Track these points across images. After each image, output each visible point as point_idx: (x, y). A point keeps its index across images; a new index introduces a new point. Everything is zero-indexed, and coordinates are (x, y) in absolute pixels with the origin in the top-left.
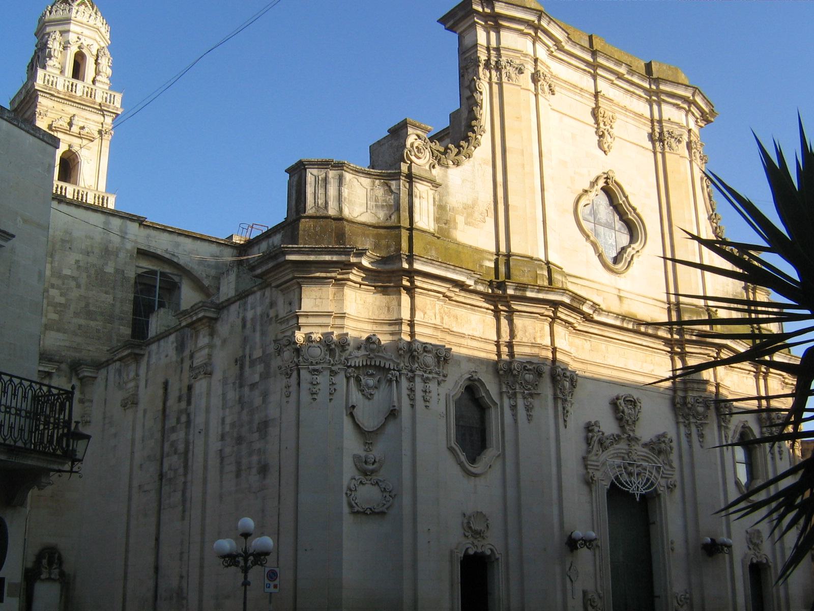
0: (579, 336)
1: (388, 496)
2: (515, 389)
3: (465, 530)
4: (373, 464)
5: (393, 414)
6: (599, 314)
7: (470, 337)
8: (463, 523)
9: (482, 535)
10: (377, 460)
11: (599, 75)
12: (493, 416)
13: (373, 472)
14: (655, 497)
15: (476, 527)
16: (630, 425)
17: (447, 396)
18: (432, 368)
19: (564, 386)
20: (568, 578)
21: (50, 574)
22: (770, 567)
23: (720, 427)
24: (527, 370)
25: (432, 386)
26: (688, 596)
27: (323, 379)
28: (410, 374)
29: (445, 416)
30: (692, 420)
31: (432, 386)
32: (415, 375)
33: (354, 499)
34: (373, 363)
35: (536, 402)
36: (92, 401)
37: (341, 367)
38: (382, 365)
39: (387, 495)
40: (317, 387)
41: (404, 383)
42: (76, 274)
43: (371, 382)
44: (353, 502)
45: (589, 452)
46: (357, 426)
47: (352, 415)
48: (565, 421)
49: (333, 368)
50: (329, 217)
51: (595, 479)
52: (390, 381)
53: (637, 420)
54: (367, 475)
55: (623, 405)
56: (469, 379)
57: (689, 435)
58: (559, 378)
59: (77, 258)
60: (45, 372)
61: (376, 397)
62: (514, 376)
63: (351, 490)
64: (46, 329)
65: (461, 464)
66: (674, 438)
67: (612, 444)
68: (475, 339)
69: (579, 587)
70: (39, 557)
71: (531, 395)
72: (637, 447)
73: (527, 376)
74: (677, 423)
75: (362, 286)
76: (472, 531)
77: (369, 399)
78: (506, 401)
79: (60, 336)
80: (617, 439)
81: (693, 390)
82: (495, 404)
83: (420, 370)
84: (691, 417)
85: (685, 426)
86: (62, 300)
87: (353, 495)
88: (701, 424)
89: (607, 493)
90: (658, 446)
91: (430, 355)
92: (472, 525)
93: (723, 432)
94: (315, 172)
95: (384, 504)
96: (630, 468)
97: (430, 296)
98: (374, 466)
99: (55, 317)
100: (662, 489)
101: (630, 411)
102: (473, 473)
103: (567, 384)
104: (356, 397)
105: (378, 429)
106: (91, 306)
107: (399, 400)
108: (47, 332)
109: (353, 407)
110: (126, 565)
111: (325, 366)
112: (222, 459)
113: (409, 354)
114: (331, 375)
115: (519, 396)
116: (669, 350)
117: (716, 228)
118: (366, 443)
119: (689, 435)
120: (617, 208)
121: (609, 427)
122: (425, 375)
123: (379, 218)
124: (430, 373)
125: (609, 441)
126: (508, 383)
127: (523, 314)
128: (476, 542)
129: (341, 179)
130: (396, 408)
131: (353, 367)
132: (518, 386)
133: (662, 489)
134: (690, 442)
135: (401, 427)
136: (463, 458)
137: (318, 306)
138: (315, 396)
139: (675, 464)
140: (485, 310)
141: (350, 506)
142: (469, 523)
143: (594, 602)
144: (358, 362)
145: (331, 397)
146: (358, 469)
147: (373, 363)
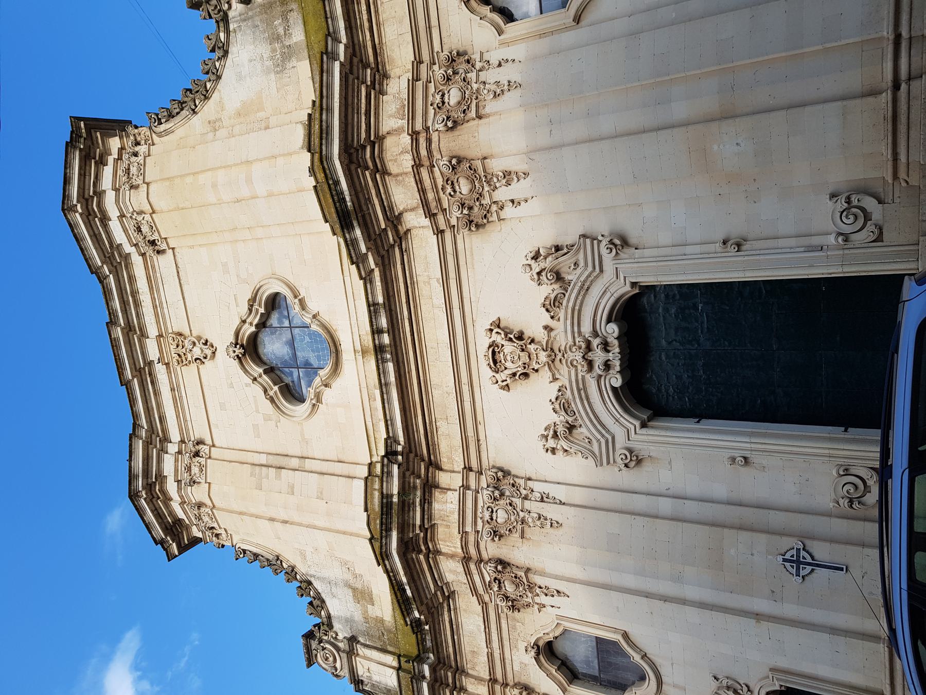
0: (436, 443)
7: (489, 646)
30: (486, 201)
68: (489, 639)
140: (452, 612)
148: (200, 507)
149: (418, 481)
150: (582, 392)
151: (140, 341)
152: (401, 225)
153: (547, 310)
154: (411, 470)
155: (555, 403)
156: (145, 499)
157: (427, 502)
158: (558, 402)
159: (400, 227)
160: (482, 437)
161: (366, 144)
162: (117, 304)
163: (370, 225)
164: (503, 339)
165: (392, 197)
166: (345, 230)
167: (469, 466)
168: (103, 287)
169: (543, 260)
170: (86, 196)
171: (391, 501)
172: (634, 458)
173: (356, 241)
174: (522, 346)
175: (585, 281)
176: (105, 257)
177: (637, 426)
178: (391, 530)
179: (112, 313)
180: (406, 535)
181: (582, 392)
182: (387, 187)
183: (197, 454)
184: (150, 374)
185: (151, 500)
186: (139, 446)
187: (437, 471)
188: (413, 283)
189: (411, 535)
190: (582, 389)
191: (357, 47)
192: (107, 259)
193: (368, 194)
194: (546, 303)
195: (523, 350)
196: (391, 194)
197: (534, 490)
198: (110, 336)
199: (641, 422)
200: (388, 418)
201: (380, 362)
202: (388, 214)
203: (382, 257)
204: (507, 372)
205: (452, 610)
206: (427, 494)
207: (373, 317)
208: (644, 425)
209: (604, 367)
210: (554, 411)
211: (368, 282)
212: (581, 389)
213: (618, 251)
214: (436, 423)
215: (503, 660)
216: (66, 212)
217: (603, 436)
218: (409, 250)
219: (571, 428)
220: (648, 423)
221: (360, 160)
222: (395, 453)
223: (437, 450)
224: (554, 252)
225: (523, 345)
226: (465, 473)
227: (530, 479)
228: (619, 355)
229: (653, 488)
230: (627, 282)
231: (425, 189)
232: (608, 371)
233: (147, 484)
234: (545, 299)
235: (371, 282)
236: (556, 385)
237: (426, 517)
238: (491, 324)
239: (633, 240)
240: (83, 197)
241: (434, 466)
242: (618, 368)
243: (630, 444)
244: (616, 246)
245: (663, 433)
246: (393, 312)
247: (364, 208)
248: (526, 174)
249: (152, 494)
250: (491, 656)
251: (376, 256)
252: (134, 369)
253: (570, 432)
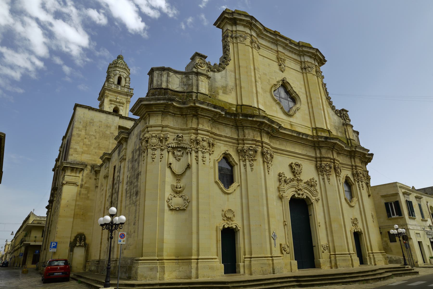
1: (186, 202)
2: (245, 158)
3: (223, 217)
4: (180, 188)
5: (189, 167)
6: (281, 129)
8: (222, 214)
9: (231, 219)
10: (182, 187)
11: (278, 44)
12: (236, 169)
13: (180, 192)
14: (311, 204)
15: (228, 215)
16: (298, 174)
17: (214, 160)
18: (206, 147)
19: (267, 157)
20: (272, 238)
21: (80, 243)
22: (362, 233)
23: (336, 176)
24: (250, 150)
25: (207, 155)
26: (328, 246)
27: (158, 152)
28: (196, 150)
29: (213, 168)
30: (324, 173)
31: (207, 155)
32: (198, 150)
33: (171, 203)
34: (180, 146)
35: (255, 163)
36: (99, 179)
37: (165, 147)
38: (184, 146)
39: (186, 202)
40: (155, 156)
41: (194, 154)
42: (95, 134)
43: (179, 154)
44: (170, 205)
45: (280, 185)
46: (173, 172)
47: (170, 167)
48: (268, 171)
49: (162, 148)
50: (162, 88)
51: (283, 196)
52: (187, 153)
53: (301, 172)
54: (177, 193)
55: (294, 166)
56: (224, 153)
57: (323, 179)
58: (264, 153)
59: (96, 129)
60: (81, 168)
61: (181, 160)
62: (245, 152)
63: (169, 200)
64: (82, 153)
65: (221, 189)
66: (318, 181)
67: (290, 182)
69: (278, 242)
70: (76, 237)
71: (252, 160)
72: (301, 183)
73: (250, 152)
74: (319, 174)
75: (176, 115)
76: (227, 218)
77: (179, 161)
78: (357, 183)
79: (88, 156)
80: (292, 180)
81: (324, 161)
82: (237, 164)
83: (201, 148)
84: (324, 172)
85: (322, 175)
86: (89, 143)
87: (170, 202)
88: (328, 175)
89: (289, 202)
90: (310, 184)
91: (205, 142)
92: (226, 215)
93: (338, 178)
94: (157, 72)
95: (185, 206)
96: (299, 192)
97: (206, 119)
98: (180, 189)
99: (86, 149)
100: (314, 201)
101: (298, 169)
102: (227, 193)
103: (269, 156)
104: (172, 159)
105: (183, 174)
106: (100, 145)
107: (191, 160)
108: (83, 154)
109: (170, 164)
110: (101, 239)
111: (158, 147)
112: (126, 192)
113: (196, 142)
114: (161, 151)
115: (247, 160)
116: (313, 145)
117: (332, 107)
118: (177, 179)
119: (323, 179)
120: (288, 92)
121: (289, 175)
122: (203, 150)
123: (184, 89)
124: (205, 150)
125: (289, 180)
126: (242, 155)
127: (248, 127)
128: (228, 222)
129: (168, 76)
130: (189, 164)
131: (170, 147)
132: (246, 157)
133: (314, 201)
134: (324, 182)
135: (192, 172)
136: (222, 186)
137: (156, 123)
138: (154, 160)
139: (319, 190)
141: (169, 207)
142: (225, 214)
143: (285, 249)
144: (174, 145)
145: (161, 160)
146: (173, 191)
147: (180, 146)
151: (283, 46)
175: (312, 192)
184: (274, 43)
215: (220, 140)
240: (316, 55)
242: (299, 197)
250: (221, 136)
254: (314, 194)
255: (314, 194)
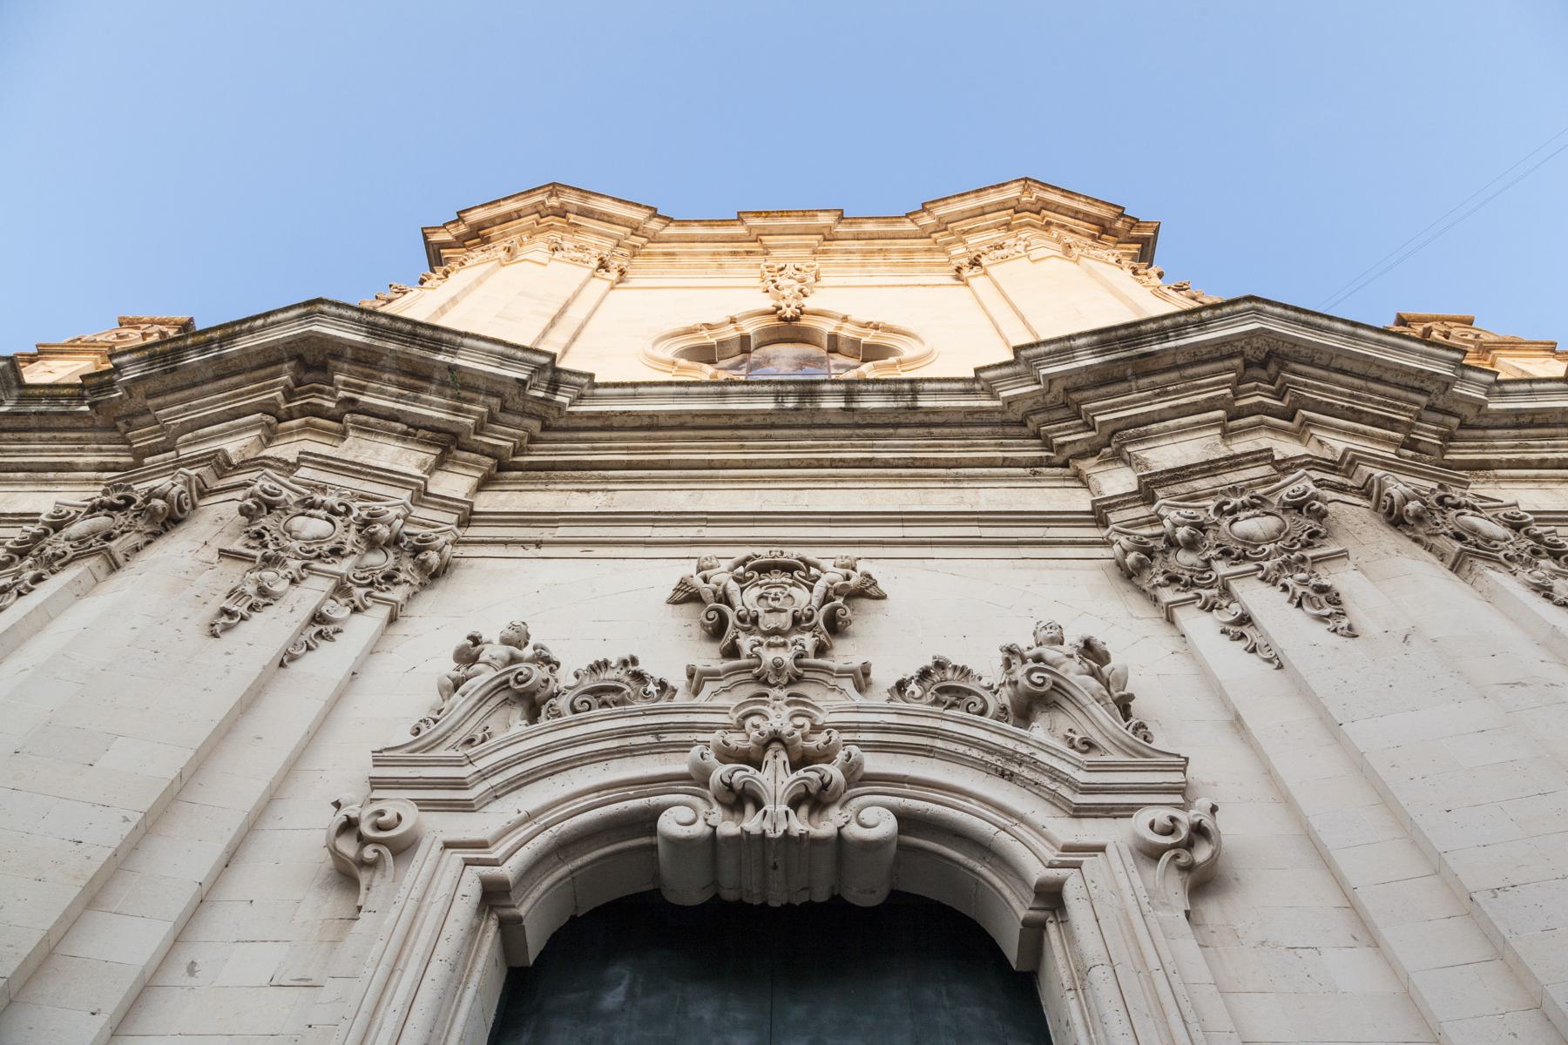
0: (550, 487)
148: (509, 251)
149: (470, 421)
150: (650, 739)
152: (1099, 464)
153: (924, 674)
154: (501, 416)
155: (624, 671)
156: (543, 203)
157: (411, 430)
158: (627, 679)
159: (1094, 460)
160: (545, 551)
161: (1287, 399)
162: (870, 227)
163: (1103, 391)
164: (832, 584)
165: (1169, 441)
166: (1095, 338)
167: (476, 520)
168: (899, 217)
169: (1086, 666)
170: (1044, 212)
171: (440, 350)
172: (369, 853)
173: (1069, 359)
174: (809, 619)
175: (1035, 765)
176: (947, 223)
177: (497, 869)
178: (371, 334)
179: (855, 220)
180: (346, 366)
181: (650, 739)
182: (1194, 430)
183: (603, 265)
185: (540, 211)
186: (638, 215)
187: (479, 475)
188: (957, 478)
189: (339, 377)
190: (659, 740)
191: (1479, 433)
192: (944, 227)
193: (1176, 392)
194: (949, 674)
195: (796, 621)
196: (1176, 439)
197: (357, 617)
198: (821, 211)
199: (507, 883)
200: (641, 390)
201: (779, 388)
202: (1131, 431)
203: (1022, 422)
204: (733, 587)
205: (100, 474)
206: (430, 434)
207: (886, 387)
208: (493, 895)
209: (738, 787)
210: (598, 664)
211: (968, 386)
212: (658, 738)
213: (1166, 857)
214: (603, 490)
216: (1023, 182)
217: (483, 776)
218: (1037, 480)
219: (533, 704)
220: (495, 916)
221: (1253, 384)
222: (554, 386)
223: (532, 487)
224: (1116, 695)
225: (813, 622)
226: (464, 505)
227: (392, 620)
228: (779, 834)
229: (224, 920)
230: (1063, 872)
231: (1215, 475)
232: (722, 804)
233: (567, 212)
234: (963, 669)
235: (966, 392)
236: (678, 679)
237: (372, 420)
238: (869, 576)
239: (1212, 910)
241: (493, 472)
243: (425, 857)
244: (1189, 845)
245: (446, 950)
246: (891, 431)
247: (1144, 381)
248: (1351, 633)
249: (548, 215)
251: (1028, 404)
252: (761, 232)
253: (520, 696)
254: (459, 784)
255: (465, 772)
